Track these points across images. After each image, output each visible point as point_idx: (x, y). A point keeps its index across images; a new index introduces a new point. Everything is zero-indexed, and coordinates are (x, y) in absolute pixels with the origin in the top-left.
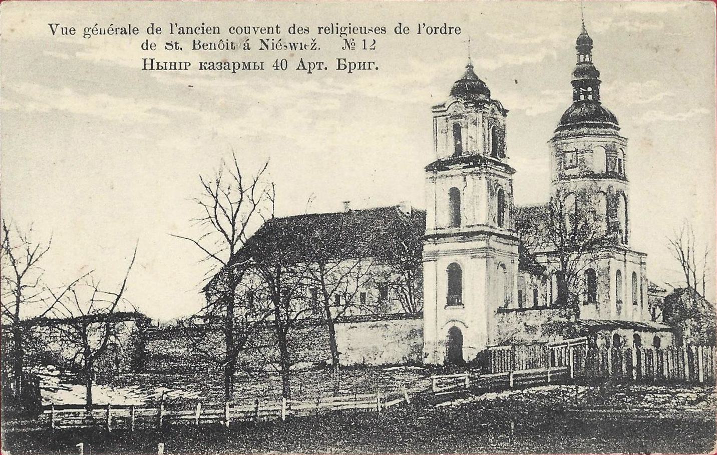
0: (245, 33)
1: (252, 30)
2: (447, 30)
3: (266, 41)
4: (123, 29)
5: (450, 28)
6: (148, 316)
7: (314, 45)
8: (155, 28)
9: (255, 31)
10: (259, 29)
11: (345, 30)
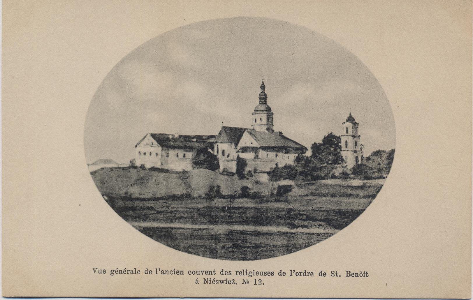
0: (197, 274)
1: (200, 273)
2: (306, 274)
3: (206, 280)
4: (132, 271)
5: (308, 273)
6: (324, 138)
7: (233, 282)
8: (255, 272)
9: (94, 270)
10: (204, 272)
11: (251, 273)
